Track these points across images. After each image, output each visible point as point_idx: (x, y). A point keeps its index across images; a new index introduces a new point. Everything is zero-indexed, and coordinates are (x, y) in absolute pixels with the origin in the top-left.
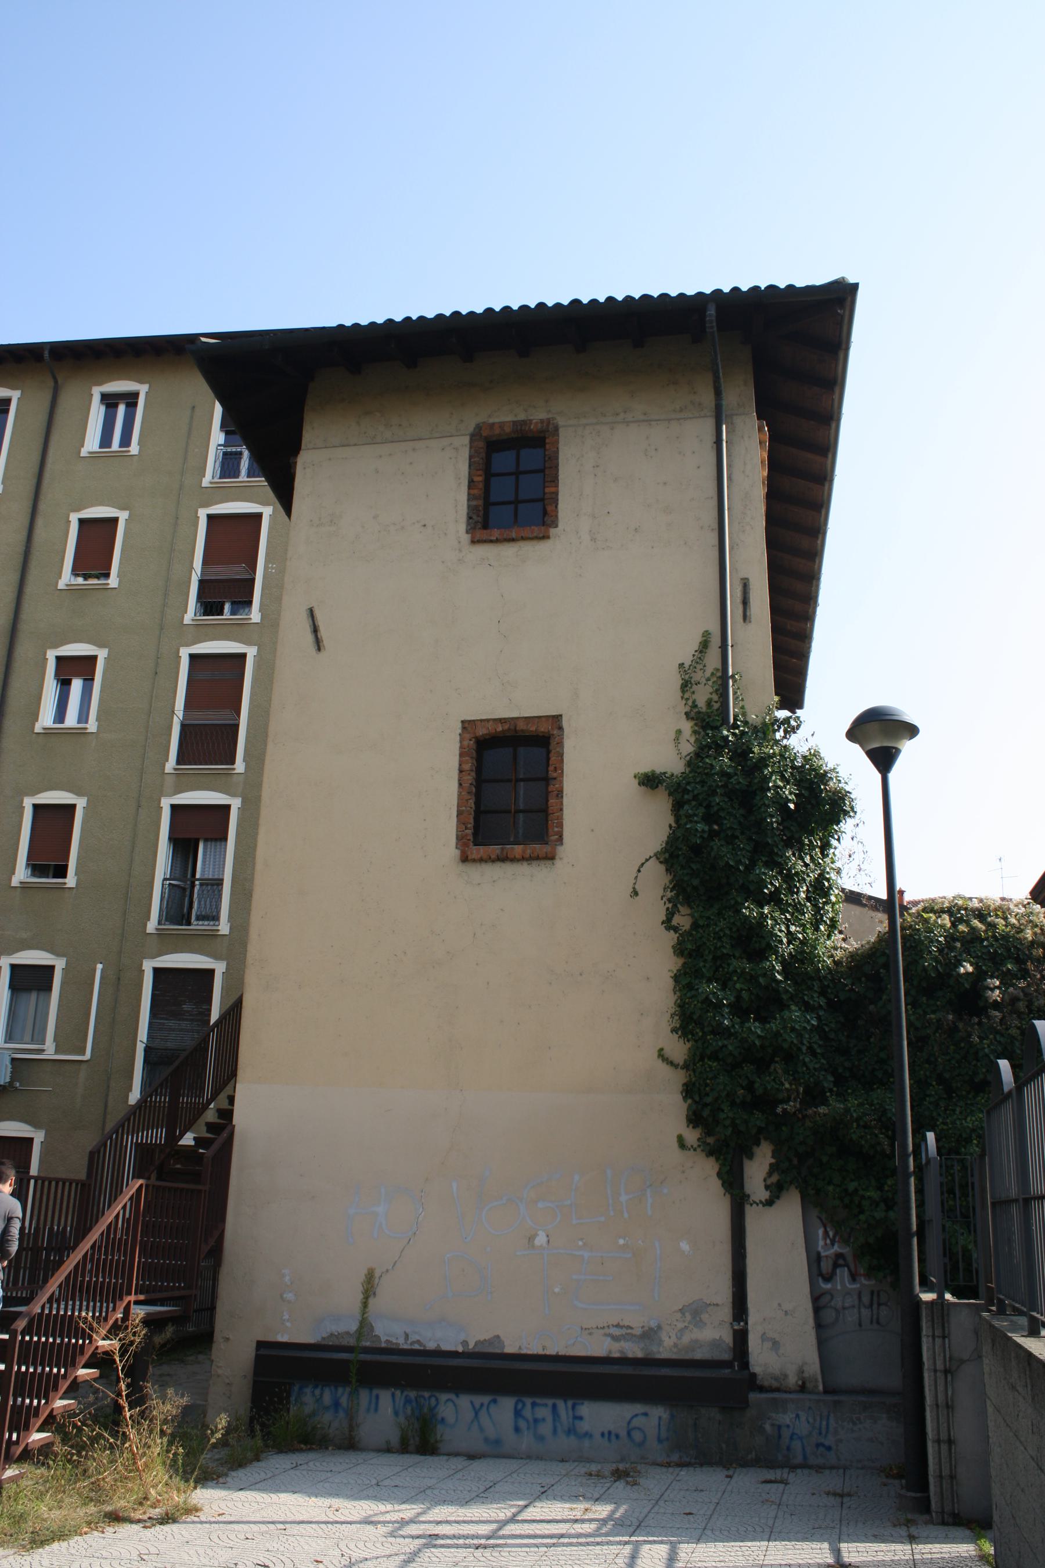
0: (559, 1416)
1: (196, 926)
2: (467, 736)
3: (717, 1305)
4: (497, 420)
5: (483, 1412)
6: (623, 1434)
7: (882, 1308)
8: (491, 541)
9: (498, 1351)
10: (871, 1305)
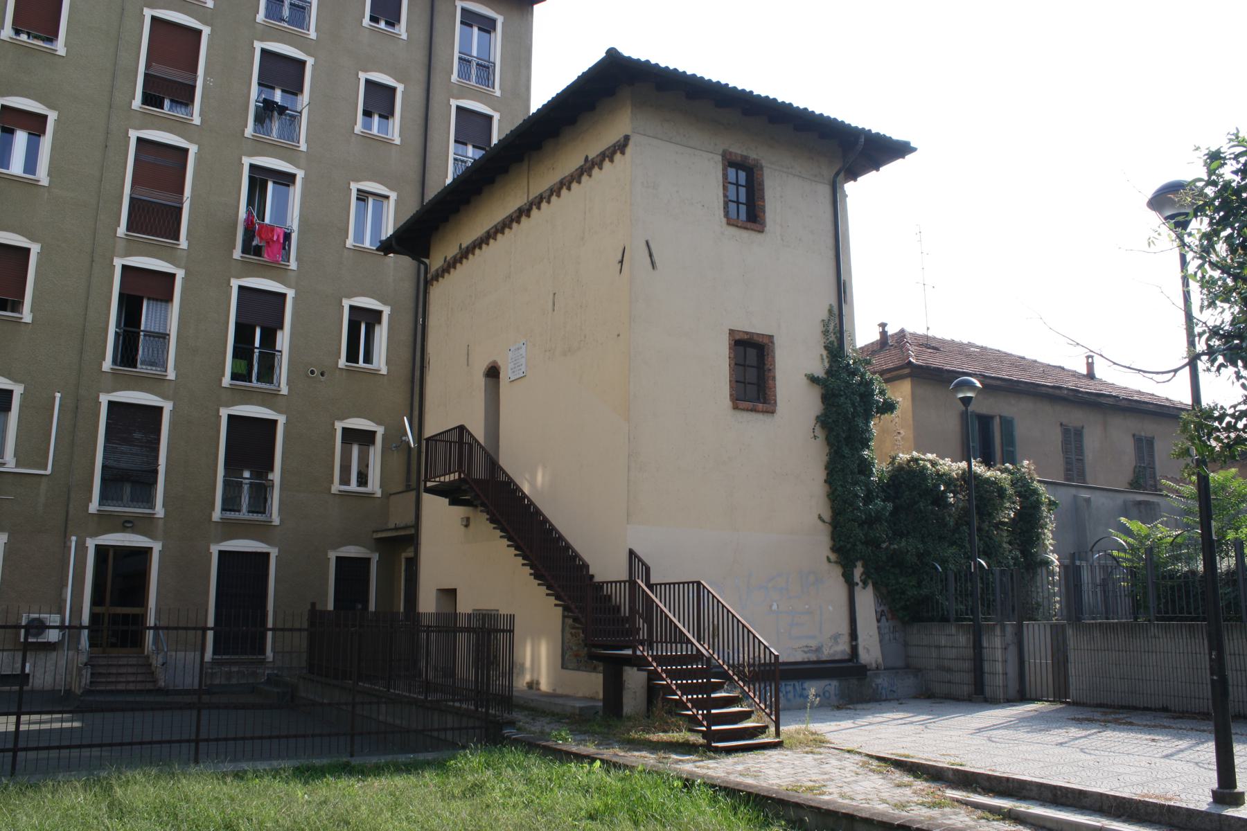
1: (141, 368)
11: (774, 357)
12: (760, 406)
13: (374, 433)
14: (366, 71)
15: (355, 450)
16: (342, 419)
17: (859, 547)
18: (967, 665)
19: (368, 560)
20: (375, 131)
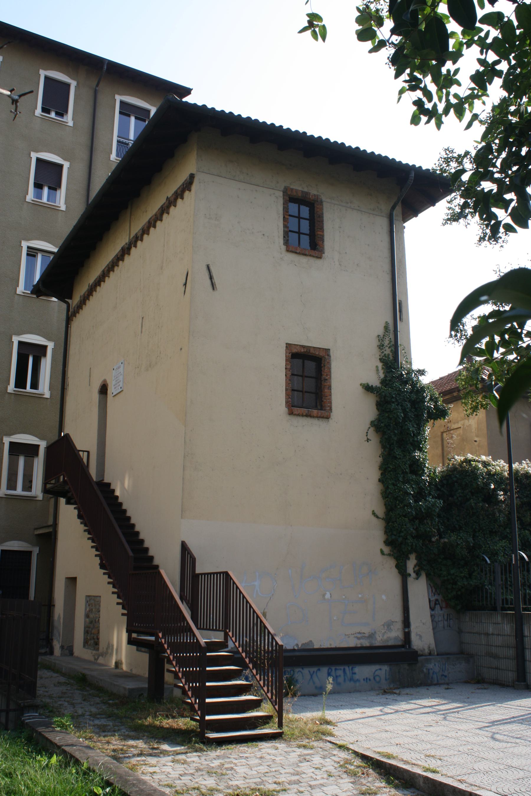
0: (346, 673)
2: (288, 351)
3: (396, 622)
4: (294, 188)
5: (315, 675)
6: (372, 678)
7: (451, 620)
8: (296, 253)
9: (312, 648)
10: (447, 620)
11: (330, 369)
12: (315, 412)
13: (38, 446)
14: (37, 151)
15: (21, 461)
16: (9, 435)
17: (410, 540)
18: (512, 652)
19: (30, 553)
20: (45, 199)
